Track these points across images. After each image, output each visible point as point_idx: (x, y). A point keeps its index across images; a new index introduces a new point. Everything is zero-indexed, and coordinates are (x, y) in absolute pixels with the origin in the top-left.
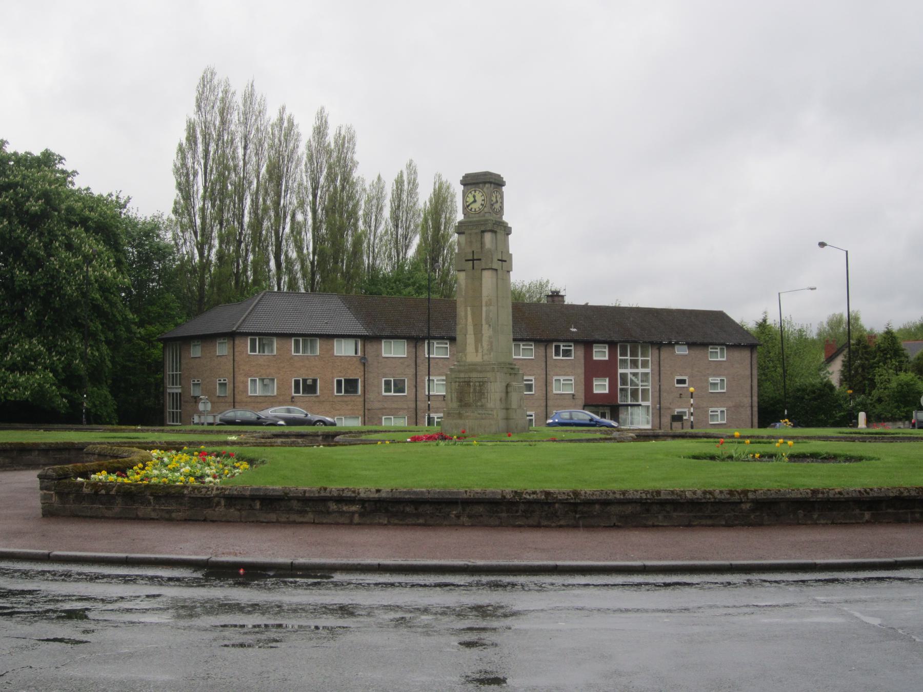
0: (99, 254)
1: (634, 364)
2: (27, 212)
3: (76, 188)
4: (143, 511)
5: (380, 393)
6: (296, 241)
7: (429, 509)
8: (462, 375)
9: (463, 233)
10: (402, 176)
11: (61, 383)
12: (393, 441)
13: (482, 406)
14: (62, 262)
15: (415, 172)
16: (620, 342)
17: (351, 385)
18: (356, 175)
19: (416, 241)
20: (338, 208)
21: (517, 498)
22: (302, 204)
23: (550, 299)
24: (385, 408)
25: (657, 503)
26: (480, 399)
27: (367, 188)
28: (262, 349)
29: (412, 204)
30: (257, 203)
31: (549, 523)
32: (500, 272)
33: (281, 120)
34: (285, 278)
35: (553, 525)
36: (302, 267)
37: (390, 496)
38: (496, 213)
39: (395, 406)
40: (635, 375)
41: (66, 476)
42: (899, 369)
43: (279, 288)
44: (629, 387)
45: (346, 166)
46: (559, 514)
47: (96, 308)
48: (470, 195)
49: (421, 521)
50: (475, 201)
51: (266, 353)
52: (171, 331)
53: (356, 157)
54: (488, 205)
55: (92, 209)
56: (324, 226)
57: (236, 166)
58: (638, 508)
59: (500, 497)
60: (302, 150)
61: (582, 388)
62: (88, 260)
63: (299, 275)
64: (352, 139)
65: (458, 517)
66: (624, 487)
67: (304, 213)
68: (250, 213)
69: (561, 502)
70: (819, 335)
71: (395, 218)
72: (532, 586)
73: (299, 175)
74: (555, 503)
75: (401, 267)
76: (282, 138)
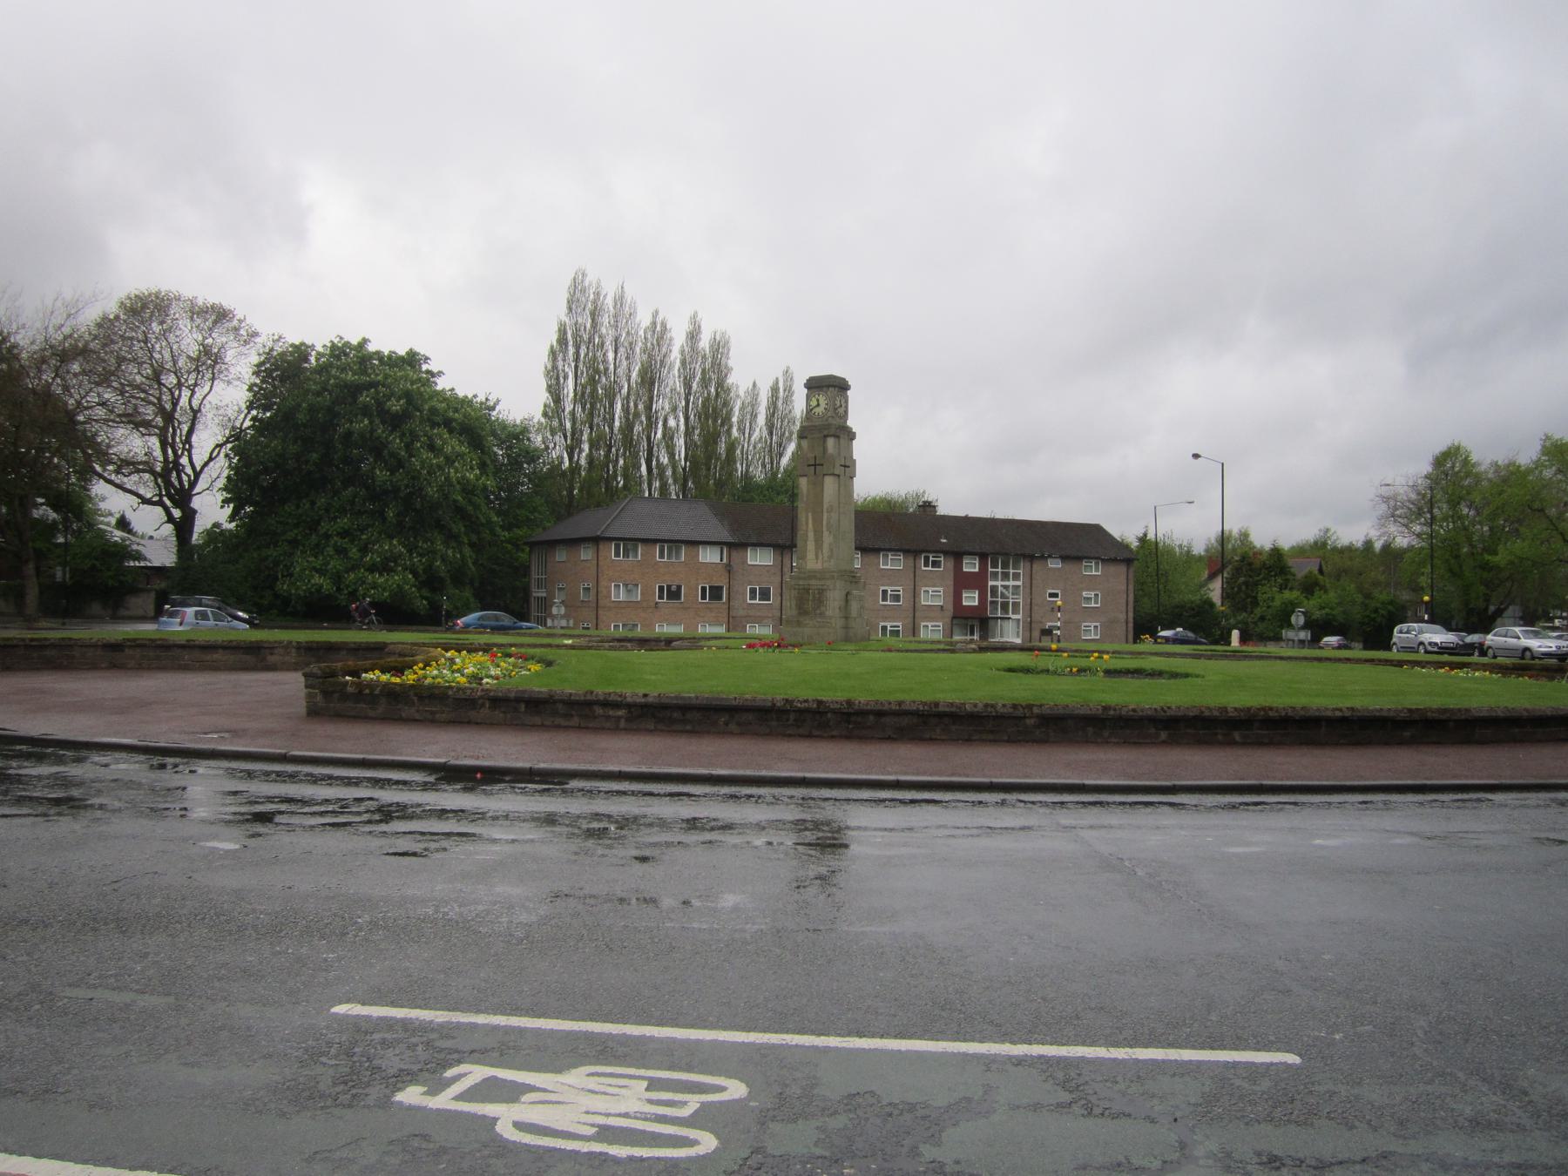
0: (460, 456)
1: (1006, 576)
2: (388, 412)
3: (439, 388)
4: (407, 712)
6: (668, 447)
11: (422, 585)
12: (718, 648)
14: (423, 462)
17: (716, 593)
18: (730, 380)
19: (791, 448)
20: (712, 413)
22: (674, 409)
28: (626, 555)
33: (654, 323)
36: (674, 472)
40: (1006, 587)
41: (333, 674)
42: (1282, 588)
47: (459, 510)
49: (688, 727)
52: (539, 535)
53: (731, 363)
55: (456, 410)
57: (606, 369)
60: (675, 356)
62: (450, 461)
69: (834, 712)
70: (1207, 550)
71: (770, 427)
73: (672, 380)
75: (774, 475)
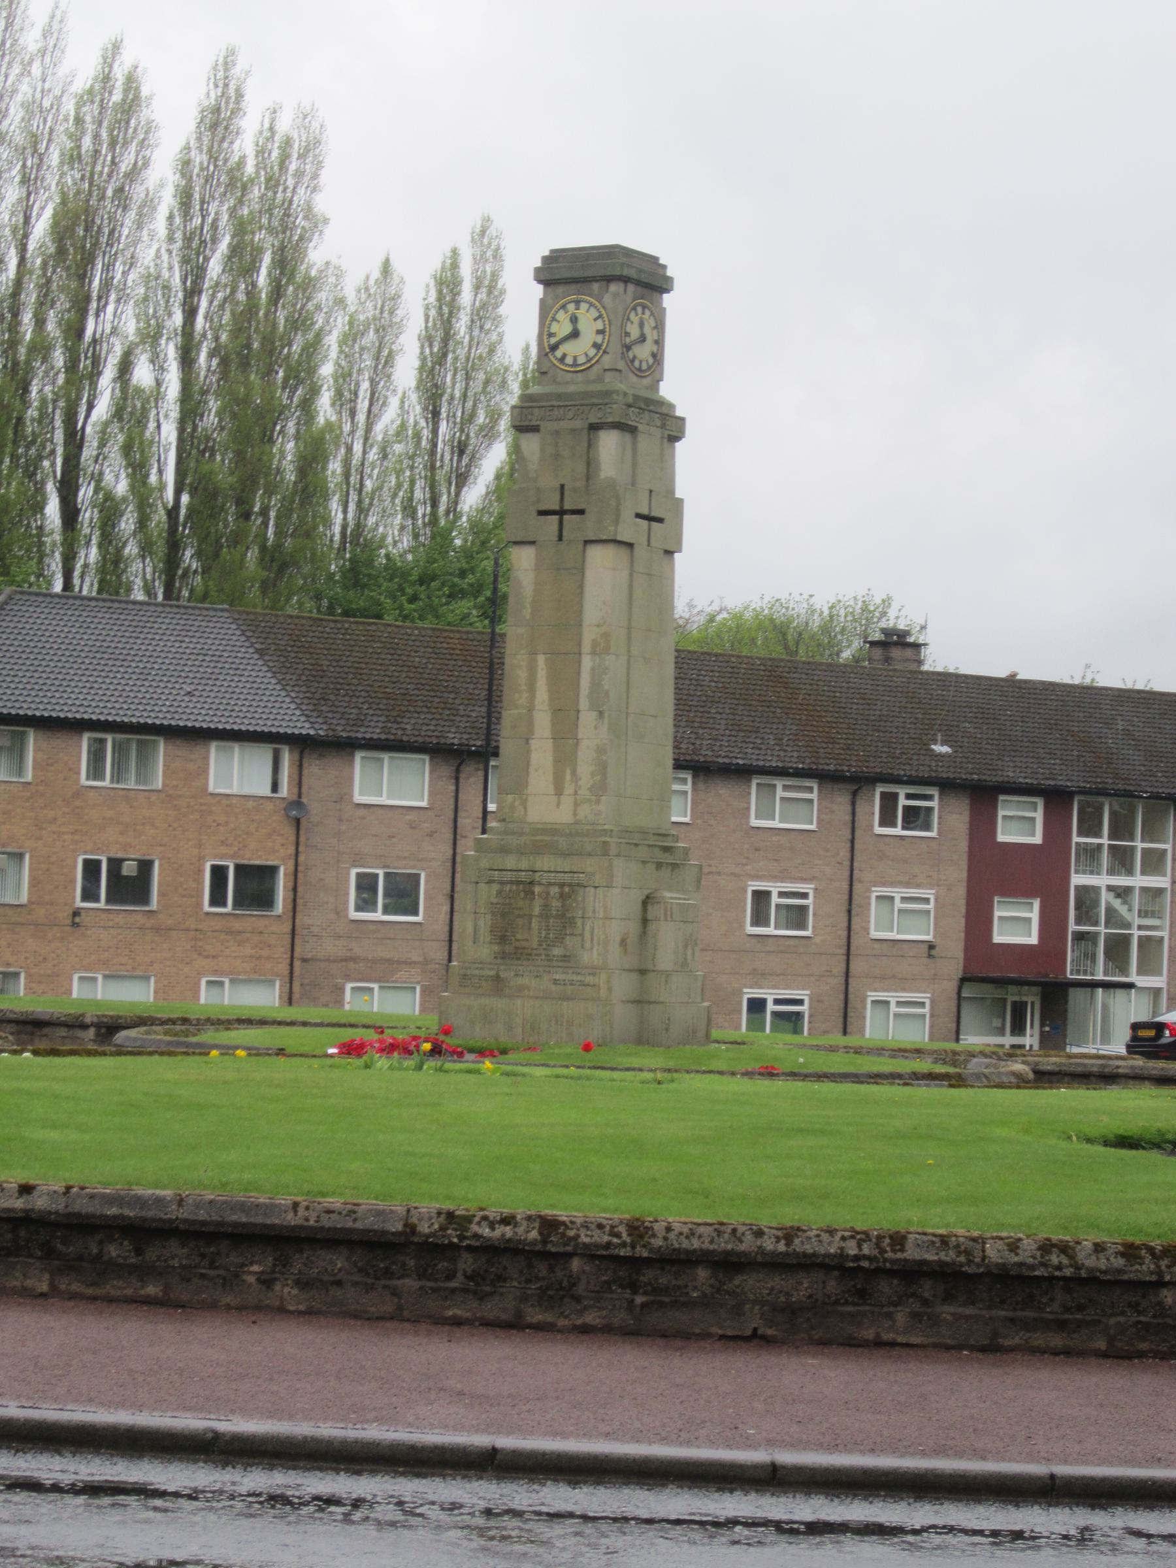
1: (1122, 860)
5: (340, 912)
7: (177, 1254)
8: (511, 862)
9: (535, 429)
10: (455, 266)
13: (565, 958)
15: (497, 256)
16: (1083, 792)
18: (317, 255)
21: (453, 1236)
22: (151, 337)
23: (878, 653)
24: (354, 959)
25: (891, 1273)
26: (560, 939)
27: (350, 295)
29: (482, 350)
31: (549, 1317)
32: (640, 551)
35: (562, 1322)
36: (142, 523)
37: (60, 1206)
38: (640, 372)
39: (381, 952)
40: (1123, 893)
43: (68, 585)
44: (1102, 929)
46: (580, 1290)
48: (561, 315)
49: (152, 1290)
50: (575, 334)
53: (322, 204)
54: (615, 348)
56: (213, 404)
58: (832, 1286)
59: (399, 1227)
60: (161, 176)
63: (131, 549)
64: (311, 148)
65: (266, 1282)
66: (790, 1215)
67: (157, 362)
69: (591, 1254)
71: (432, 396)
72: (389, 1513)
73: (149, 248)
74: (570, 1255)
75: (441, 537)
76: (104, 135)
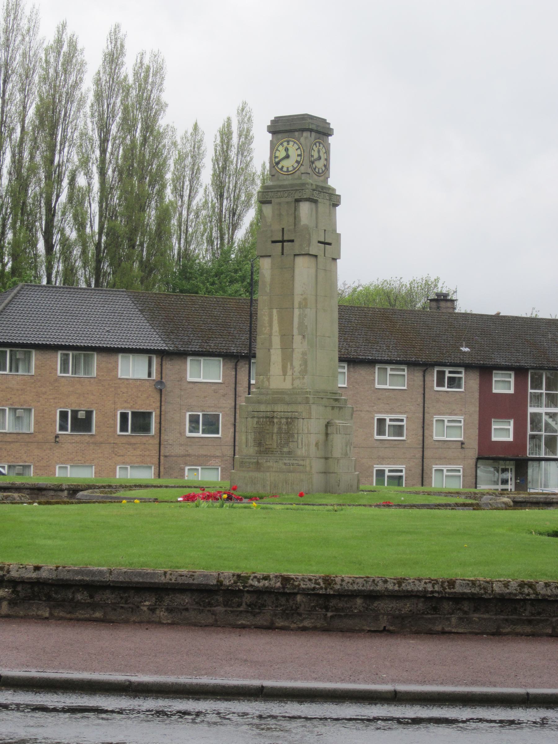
5: (182, 433)
7: (109, 597)
8: (263, 408)
9: (269, 202)
13: (289, 453)
16: (533, 368)
18: (163, 122)
21: (240, 586)
22: (85, 162)
23: (434, 304)
24: (189, 455)
25: (449, 599)
26: (287, 443)
28: (15, 367)
29: (243, 165)
30: (20, 161)
31: (286, 624)
32: (320, 259)
33: (59, 41)
34: (59, 267)
35: (293, 626)
38: (318, 174)
39: (202, 452)
43: (49, 281)
44: (543, 433)
45: (149, 108)
46: (301, 610)
48: (280, 148)
49: (98, 615)
50: (287, 157)
51: (20, 373)
53: (165, 97)
54: (306, 162)
56: (117, 194)
58: (420, 605)
59: (215, 582)
60: (88, 87)
61: (475, 432)
63: (79, 264)
64: (159, 71)
65: (152, 610)
66: (400, 572)
67: (88, 174)
68: (10, 174)
69: (306, 593)
71: (220, 187)
73: (83, 121)
74: (295, 594)
75: (226, 254)
